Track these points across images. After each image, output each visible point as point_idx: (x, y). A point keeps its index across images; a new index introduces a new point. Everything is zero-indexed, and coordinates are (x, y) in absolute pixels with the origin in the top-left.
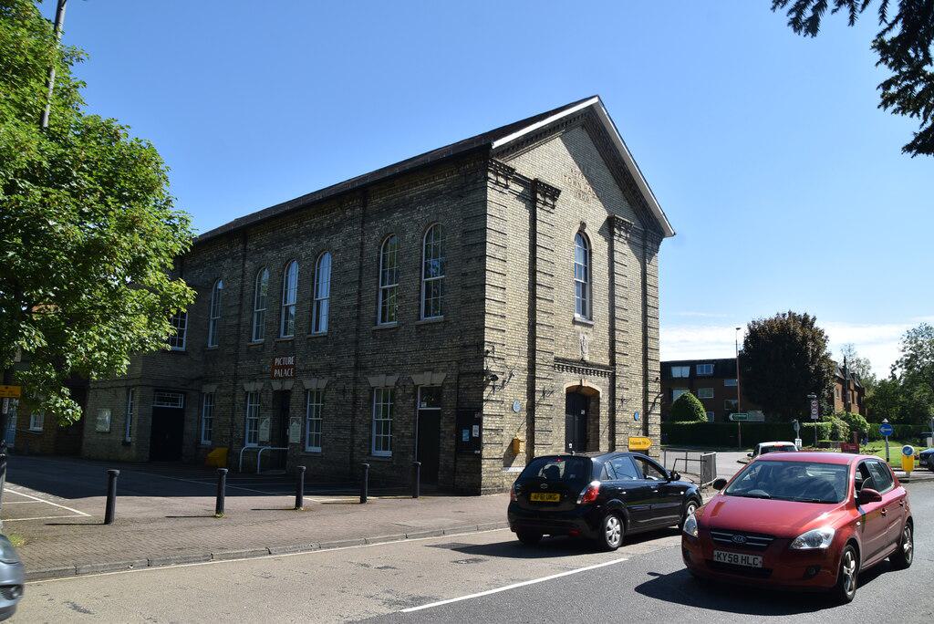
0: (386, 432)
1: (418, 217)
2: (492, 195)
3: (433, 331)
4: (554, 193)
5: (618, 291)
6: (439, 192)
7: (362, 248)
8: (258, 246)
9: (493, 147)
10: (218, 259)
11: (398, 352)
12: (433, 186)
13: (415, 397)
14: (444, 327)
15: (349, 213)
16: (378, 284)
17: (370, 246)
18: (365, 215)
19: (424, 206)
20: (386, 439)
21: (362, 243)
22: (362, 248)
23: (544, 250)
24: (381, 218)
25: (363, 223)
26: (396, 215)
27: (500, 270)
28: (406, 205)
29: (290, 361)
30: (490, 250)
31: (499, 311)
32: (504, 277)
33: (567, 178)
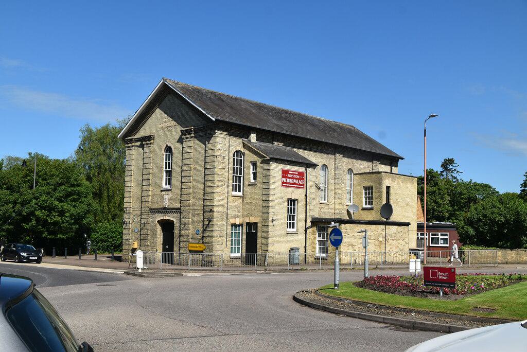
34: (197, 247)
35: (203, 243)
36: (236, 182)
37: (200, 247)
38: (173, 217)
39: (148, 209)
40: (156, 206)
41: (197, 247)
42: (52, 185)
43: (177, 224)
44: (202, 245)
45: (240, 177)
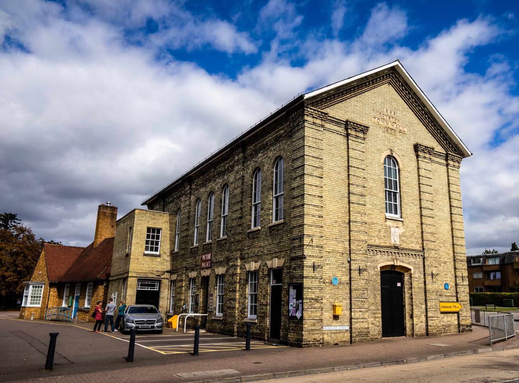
0: (256, 302)
1: (270, 154)
2: (309, 132)
3: (278, 231)
4: (364, 129)
5: (425, 197)
6: (281, 136)
7: (243, 180)
8: (197, 186)
9: (305, 98)
10: (180, 196)
11: (260, 247)
12: (277, 132)
13: (269, 277)
14: (284, 227)
15: (236, 158)
16: (251, 202)
17: (247, 177)
18: (244, 157)
19: (273, 147)
20: (255, 306)
21: (243, 176)
22: (243, 180)
23: (355, 169)
24: (252, 158)
25: (244, 163)
26: (260, 155)
27: (317, 183)
28: (265, 148)
29: (209, 256)
30: (308, 170)
31: (317, 212)
32: (321, 189)
33: (376, 119)
34: (451, 307)
35: (457, 301)
36: (390, 200)
37: (455, 307)
38: (409, 264)
39: (365, 246)
40: (377, 242)
41: (451, 307)
42: (296, 177)
43: (417, 274)
44: (457, 304)
45: (395, 194)
